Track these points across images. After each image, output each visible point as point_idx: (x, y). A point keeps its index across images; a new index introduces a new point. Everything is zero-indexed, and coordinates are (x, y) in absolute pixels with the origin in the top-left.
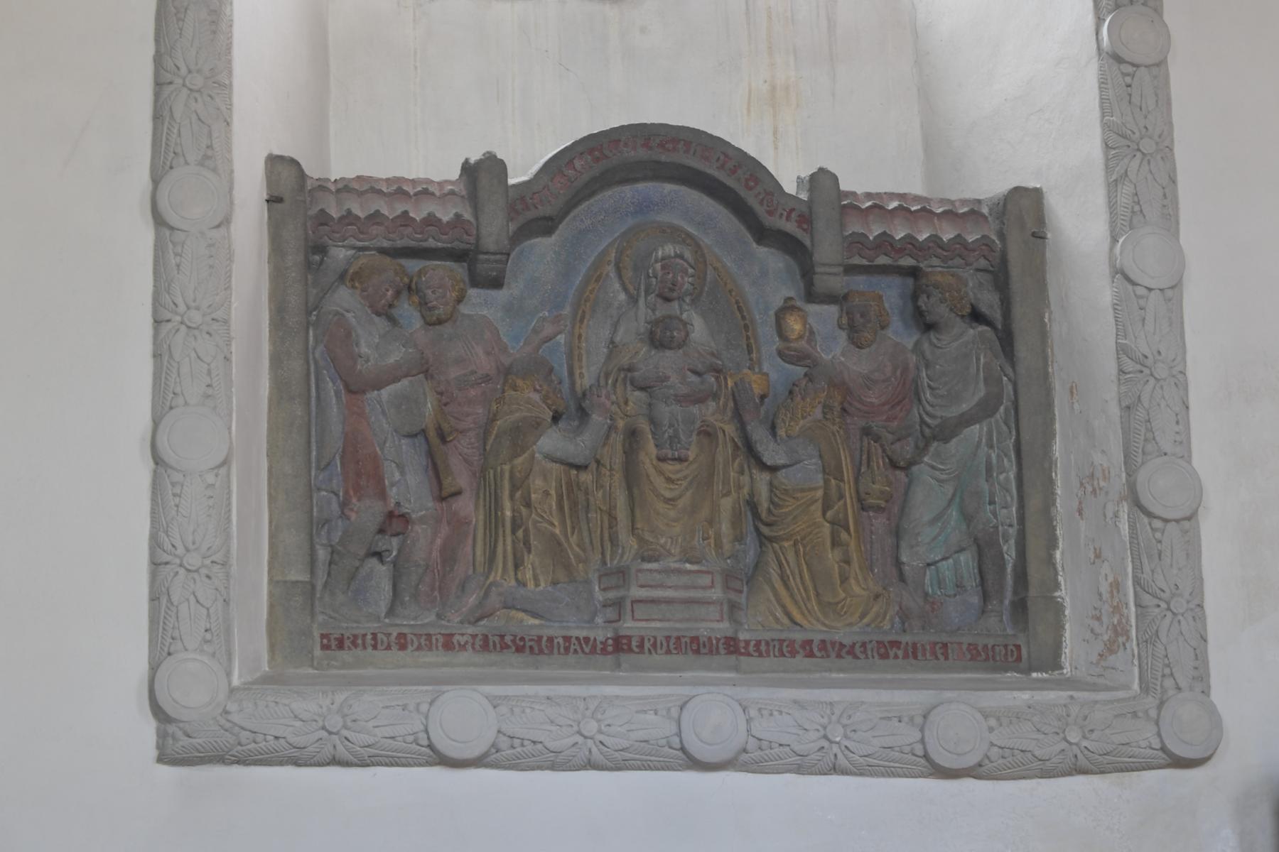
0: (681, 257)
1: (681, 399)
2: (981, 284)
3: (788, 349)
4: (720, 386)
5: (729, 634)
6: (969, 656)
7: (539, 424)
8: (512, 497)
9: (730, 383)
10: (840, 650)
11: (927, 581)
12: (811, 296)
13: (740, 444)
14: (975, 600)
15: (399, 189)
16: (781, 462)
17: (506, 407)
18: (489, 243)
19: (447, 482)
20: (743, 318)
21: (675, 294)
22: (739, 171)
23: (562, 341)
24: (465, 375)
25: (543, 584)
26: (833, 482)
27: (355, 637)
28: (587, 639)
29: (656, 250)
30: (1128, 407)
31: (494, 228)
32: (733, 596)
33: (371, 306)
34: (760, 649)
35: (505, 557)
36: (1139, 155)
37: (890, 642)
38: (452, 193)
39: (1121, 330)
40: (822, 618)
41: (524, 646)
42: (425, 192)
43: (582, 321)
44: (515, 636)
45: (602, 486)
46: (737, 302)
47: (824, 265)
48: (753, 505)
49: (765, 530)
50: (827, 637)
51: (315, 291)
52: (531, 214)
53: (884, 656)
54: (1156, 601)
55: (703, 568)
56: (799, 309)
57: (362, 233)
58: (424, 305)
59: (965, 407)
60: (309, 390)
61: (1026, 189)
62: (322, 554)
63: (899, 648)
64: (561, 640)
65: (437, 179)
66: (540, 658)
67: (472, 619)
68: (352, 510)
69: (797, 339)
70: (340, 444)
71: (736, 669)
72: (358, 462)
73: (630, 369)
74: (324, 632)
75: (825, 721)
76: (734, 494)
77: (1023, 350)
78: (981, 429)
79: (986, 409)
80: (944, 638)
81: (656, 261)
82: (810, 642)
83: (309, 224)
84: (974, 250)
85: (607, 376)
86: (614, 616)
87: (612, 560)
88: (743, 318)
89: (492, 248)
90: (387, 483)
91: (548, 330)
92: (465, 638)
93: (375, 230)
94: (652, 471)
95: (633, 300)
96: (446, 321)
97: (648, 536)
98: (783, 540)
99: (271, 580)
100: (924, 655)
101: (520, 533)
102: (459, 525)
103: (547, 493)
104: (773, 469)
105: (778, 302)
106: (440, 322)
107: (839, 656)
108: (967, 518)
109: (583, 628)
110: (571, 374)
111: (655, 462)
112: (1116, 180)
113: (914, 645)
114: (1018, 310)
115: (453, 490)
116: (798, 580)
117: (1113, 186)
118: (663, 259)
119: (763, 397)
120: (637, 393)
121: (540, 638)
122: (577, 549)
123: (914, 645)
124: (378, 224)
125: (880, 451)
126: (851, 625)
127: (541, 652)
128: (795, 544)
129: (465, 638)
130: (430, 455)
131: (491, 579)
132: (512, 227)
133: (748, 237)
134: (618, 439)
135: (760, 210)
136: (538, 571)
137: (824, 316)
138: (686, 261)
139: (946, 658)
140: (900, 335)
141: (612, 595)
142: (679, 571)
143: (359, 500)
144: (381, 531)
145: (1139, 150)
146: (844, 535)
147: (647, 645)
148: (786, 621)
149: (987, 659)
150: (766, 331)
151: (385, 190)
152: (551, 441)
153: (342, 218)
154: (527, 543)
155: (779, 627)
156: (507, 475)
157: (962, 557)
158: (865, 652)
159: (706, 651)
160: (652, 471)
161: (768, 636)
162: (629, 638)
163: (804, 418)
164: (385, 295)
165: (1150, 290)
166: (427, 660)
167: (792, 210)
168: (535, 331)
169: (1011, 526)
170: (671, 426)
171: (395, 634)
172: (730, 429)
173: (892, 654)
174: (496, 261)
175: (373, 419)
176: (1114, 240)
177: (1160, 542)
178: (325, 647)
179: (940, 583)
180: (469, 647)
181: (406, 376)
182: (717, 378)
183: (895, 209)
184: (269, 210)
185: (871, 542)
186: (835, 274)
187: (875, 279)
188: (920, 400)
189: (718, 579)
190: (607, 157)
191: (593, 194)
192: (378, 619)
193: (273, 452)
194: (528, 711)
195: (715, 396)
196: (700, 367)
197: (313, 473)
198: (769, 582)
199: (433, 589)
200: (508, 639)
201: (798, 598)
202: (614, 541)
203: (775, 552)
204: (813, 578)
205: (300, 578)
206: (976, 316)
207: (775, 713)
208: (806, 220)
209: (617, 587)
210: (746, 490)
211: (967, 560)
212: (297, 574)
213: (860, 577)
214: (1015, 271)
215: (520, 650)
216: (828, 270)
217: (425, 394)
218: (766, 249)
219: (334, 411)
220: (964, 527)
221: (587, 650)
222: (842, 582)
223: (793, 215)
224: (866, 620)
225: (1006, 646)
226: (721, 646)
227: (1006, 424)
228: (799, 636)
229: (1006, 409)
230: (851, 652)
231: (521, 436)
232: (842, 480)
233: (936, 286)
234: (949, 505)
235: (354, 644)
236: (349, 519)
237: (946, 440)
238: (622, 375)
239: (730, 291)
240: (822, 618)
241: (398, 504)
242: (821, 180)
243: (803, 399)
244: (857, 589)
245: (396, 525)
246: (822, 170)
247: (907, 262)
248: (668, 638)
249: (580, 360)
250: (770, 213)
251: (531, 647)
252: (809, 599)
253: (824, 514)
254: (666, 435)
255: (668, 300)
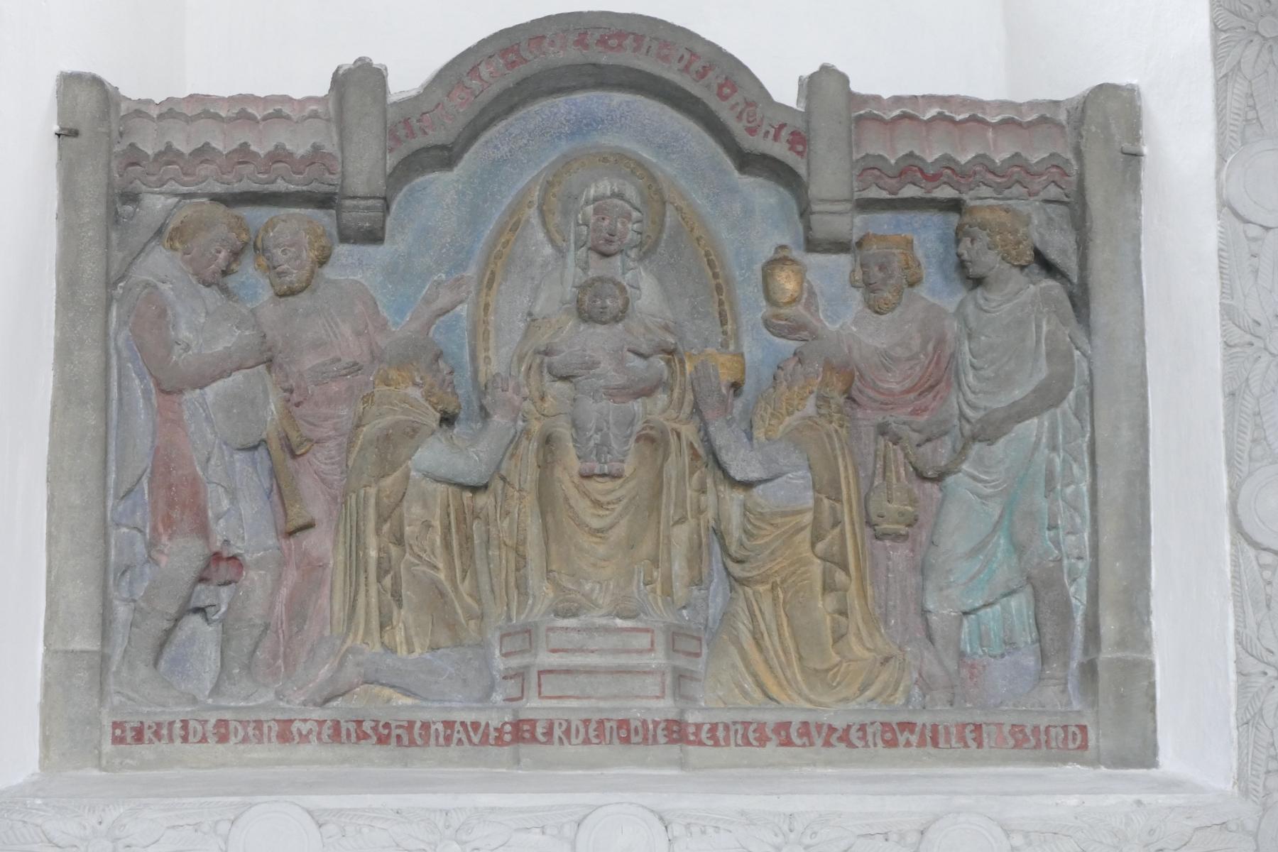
0: (620, 196)
1: (616, 393)
2: (1050, 219)
3: (777, 317)
4: (672, 373)
5: (671, 716)
6: (1012, 742)
7: (415, 431)
8: (378, 531)
9: (689, 367)
10: (828, 736)
11: (964, 634)
12: (812, 245)
13: (701, 451)
14: (1030, 661)
15: (244, 111)
16: (754, 475)
17: (374, 408)
18: (358, 184)
19: (293, 511)
20: (715, 276)
21: (613, 248)
22: (711, 74)
23: (464, 314)
24: (324, 364)
25: (418, 650)
26: (826, 502)
27: (159, 725)
28: (475, 725)
29: (587, 186)
30: (1233, 394)
31: (364, 166)
32: (682, 662)
33: (196, 274)
34: (715, 735)
35: (367, 613)
36: (1257, 39)
37: (899, 724)
38: (315, 115)
39: (1227, 289)
40: (805, 690)
41: (389, 735)
42: (278, 115)
43: (490, 286)
44: (377, 722)
45: (508, 513)
46: (707, 254)
47: (823, 201)
48: (719, 534)
49: (736, 569)
50: (811, 718)
51: (120, 255)
52: (418, 142)
53: (891, 743)
54: (1262, 667)
55: (640, 625)
56: (793, 262)
57: (185, 174)
58: (272, 269)
59: (1017, 394)
60: (107, 390)
61: (1115, 87)
62: (122, 612)
63: (912, 732)
64: (440, 727)
65: (297, 95)
66: (409, 750)
67: (319, 700)
68: (162, 552)
69: (789, 303)
70: (148, 462)
71: (682, 764)
72: (170, 488)
73: (547, 353)
74: (118, 719)
75: (779, 840)
76: (692, 522)
77: (1100, 311)
78: (1041, 425)
79: (1046, 398)
80: (979, 719)
81: (587, 203)
82: (785, 726)
83: (114, 164)
84: (1041, 175)
85: (521, 359)
86: (515, 693)
87: (518, 613)
88: (715, 276)
89: (361, 190)
90: (210, 514)
91: (444, 300)
92: (309, 725)
93: (204, 170)
94: (572, 493)
95: (561, 252)
96: (301, 290)
97: (567, 582)
98: (757, 582)
99: (47, 650)
100: (948, 741)
101: (388, 581)
102: (313, 569)
103: (428, 526)
104: (748, 485)
105: (768, 252)
106: (292, 292)
107: (827, 744)
108: (1018, 548)
109: (471, 709)
110: (474, 358)
111: (577, 479)
112: (1226, 75)
113: (935, 728)
114: (1099, 257)
115: (301, 522)
116: (776, 638)
117: (1222, 83)
118: (595, 200)
119: (736, 387)
120: (559, 384)
121: (411, 724)
122: (469, 600)
123: (935, 728)
124: (206, 161)
125: (901, 456)
126: (846, 700)
127: (412, 743)
128: (773, 589)
129: (309, 725)
130: (273, 473)
131: (349, 642)
132: (391, 161)
133: (728, 163)
134: (530, 449)
135: (738, 129)
136: (412, 632)
137: (832, 270)
138: (628, 202)
139: (980, 745)
140: (938, 294)
141: (515, 662)
142: (606, 630)
143: (170, 539)
144: (202, 579)
145: (1257, 32)
146: (840, 576)
147: (558, 732)
148: (757, 695)
149: (1037, 746)
150: (748, 293)
151: (223, 114)
152: (433, 454)
153: (159, 155)
154: (397, 596)
155: (747, 704)
156: (372, 501)
157: (1014, 602)
158: (864, 738)
159: (639, 739)
160: (572, 493)
161: (727, 717)
162: (533, 722)
163: (790, 414)
164: (216, 258)
165: (1267, 229)
166: (255, 755)
167: (782, 126)
168: (427, 301)
169: (1080, 558)
170: (599, 430)
171: (213, 721)
172: (689, 431)
173: (902, 739)
174: (368, 208)
175: (192, 428)
176: (1222, 158)
177: (1270, 583)
178: (118, 740)
179: (982, 638)
180: (313, 737)
181: (238, 369)
182: (668, 362)
183: (933, 119)
184: (60, 148)
185: (887, 582)
186: (840, 213)
187: (904, 217)
188: (959, 385)
189: (660, 639)
190: (526, 61)
191: (511, 109)
192: (194, 700)
193: (54, 477)
194: (365, 830)
195: (668, 387)
196: (644, 348)
197: (110, 503)
198: (737, 642)
199: (275, 657)
200: (367, 726)
201: (775, 662)
202: (522, 587)
203: (747, 599)
204: (794, 635)
205: (87, 647)
206: (1048, 267)
207: (710, 830)
208: (799, 140)
209: (522, 652)
210: (710, 514)
211: (1019, 604)
212: (85, 642)
213: (864, 634)
214: (1096, 200)
215: (382, 740)
216: (828, 207)
217: (265, 392)
218: (752, 179)
219: (142, 418)
220: (1014, 560)
221: (476, 739)
222: (835, 641)
223: (784, 134)
224: (869, 693)
225: (1065, 727)
226: (659, 732)
227: (1077, 415)
228: (771, 717)
229: (1078, 396)
230: (845, 738)
231: (394, 445)
232: (838, 500)
233: (983, 227)
234: (994, 530)
235: (157, 734)
236: (157, 563)
237: (991, 441)
238: (538, 361)
239: (698, 240)
240: (805, 690)
241: (226, 542)
242: (824, 83)
243: (789, 387)
244: (858, 650)
245: (224, 571)
246: (826, 70)
247: (945, 192)
248: (586, 722)
249: (486, 340)
250: (752, 131)
251: (399, 737)
252: (790, 665)
253: (813, 545)
254: (592, 443)
255: (605, 255)
